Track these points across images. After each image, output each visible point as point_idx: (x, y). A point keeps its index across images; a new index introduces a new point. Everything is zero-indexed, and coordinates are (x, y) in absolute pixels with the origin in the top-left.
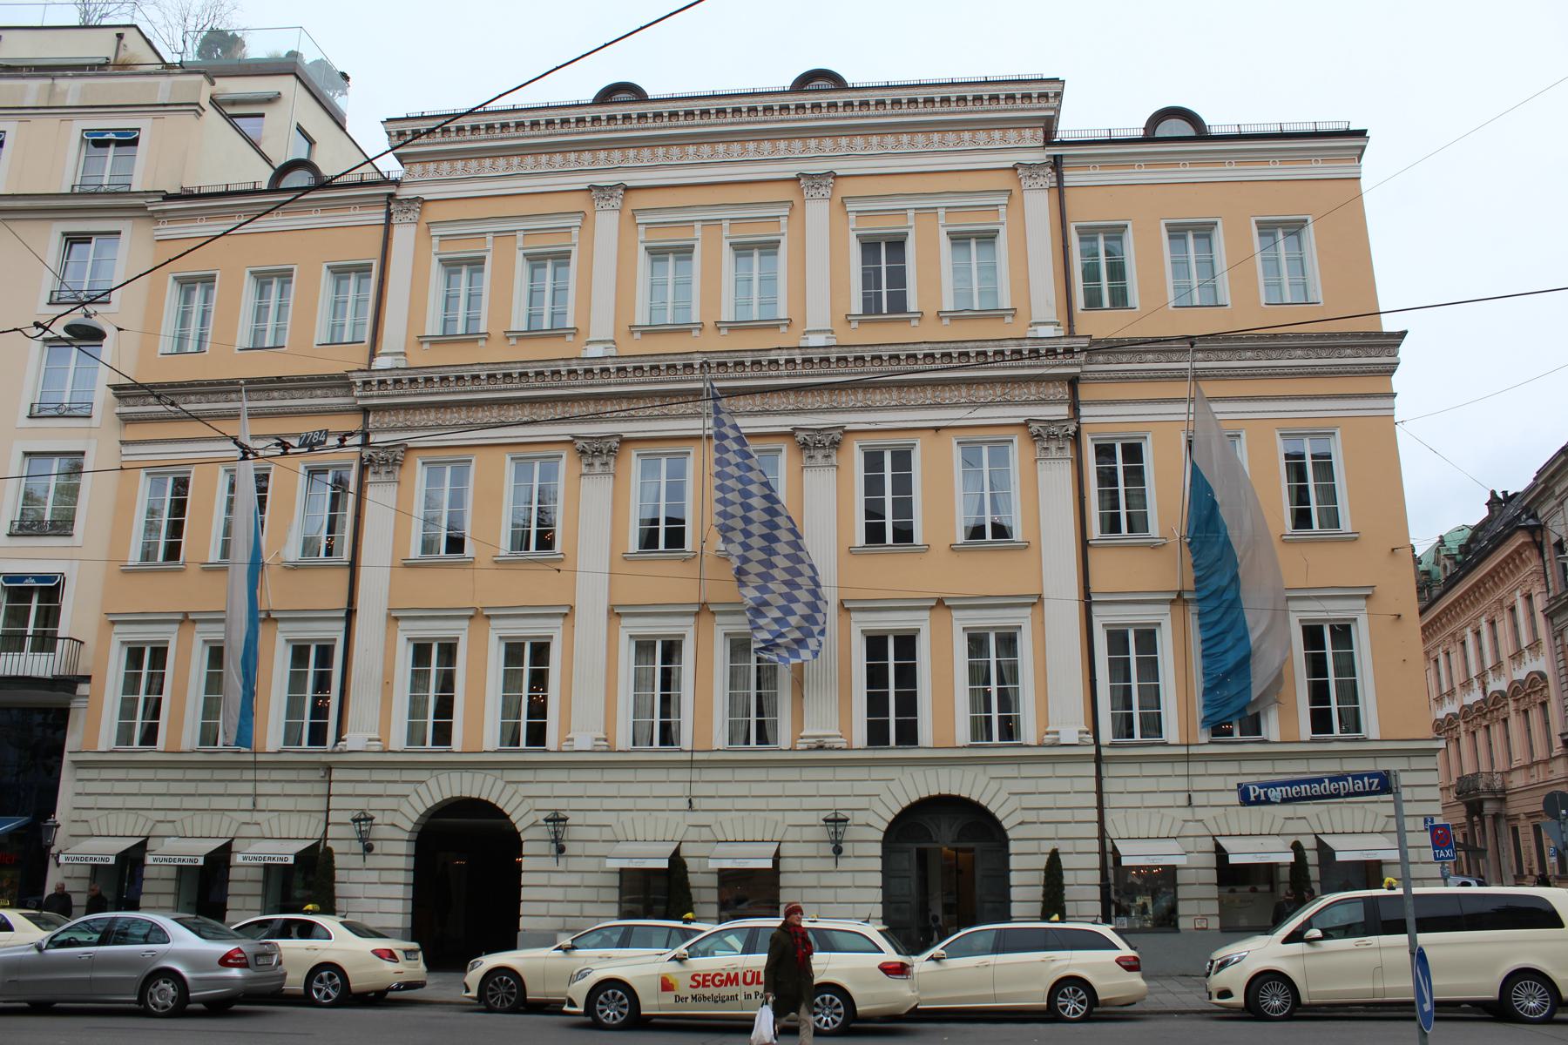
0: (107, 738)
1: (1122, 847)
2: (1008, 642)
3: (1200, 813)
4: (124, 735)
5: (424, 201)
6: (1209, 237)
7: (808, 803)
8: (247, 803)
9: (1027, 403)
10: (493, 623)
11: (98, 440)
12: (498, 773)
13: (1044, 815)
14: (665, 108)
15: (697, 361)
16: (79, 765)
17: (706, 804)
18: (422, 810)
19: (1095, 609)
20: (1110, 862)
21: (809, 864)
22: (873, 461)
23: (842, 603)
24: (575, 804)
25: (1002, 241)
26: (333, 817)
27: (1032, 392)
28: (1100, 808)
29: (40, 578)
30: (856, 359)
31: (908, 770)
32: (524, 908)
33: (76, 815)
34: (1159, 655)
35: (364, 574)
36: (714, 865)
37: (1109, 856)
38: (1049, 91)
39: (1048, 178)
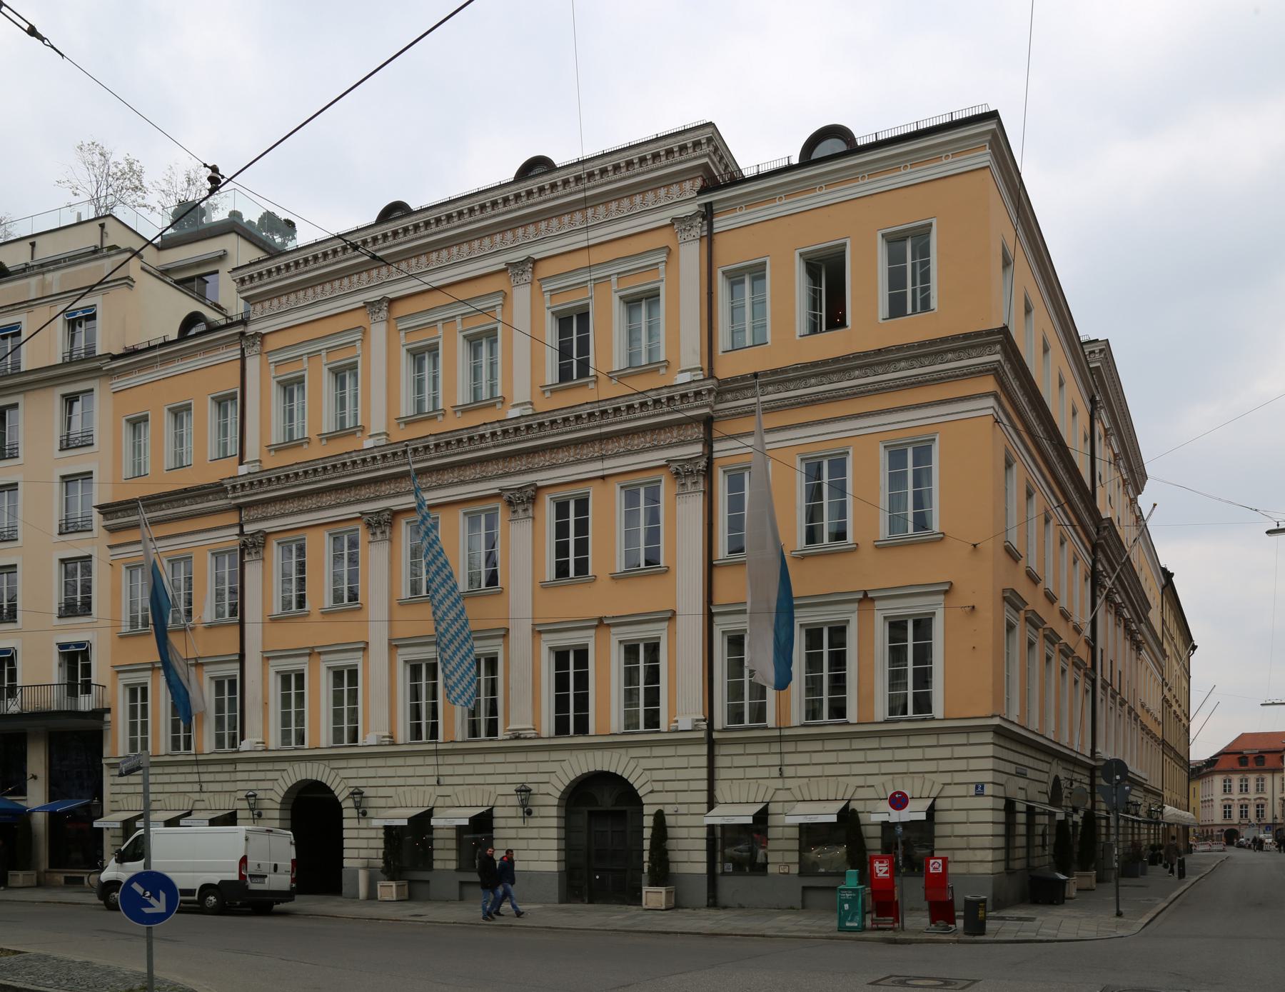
3: (789, 783)
8: (197, 788)
11: (94, 543)
13: (669, 786)
19: (717, 619)
21: (512, 823)
22: (562, 509)
23: (390, 640)
24: (372, 782)
31: (575, 753)
32: (346, 853)
35: (247, 627)
39: (698, 230)
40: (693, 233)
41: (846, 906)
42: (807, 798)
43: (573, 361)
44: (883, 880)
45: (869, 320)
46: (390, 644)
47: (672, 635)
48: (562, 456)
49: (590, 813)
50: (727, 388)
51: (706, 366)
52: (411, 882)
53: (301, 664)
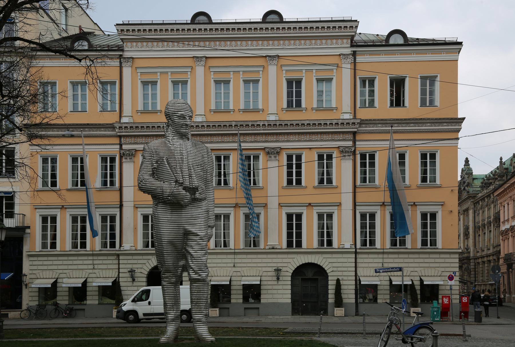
0: (38, 246)
1: (361, 279)
2: (330, 216)
4: (44, 246)
5: (133, 58)
7: (269, 265)
8: (91, 267)
9: (340, 140)
13: (339, 269)
15: (233, 124)
16: (30, 256)
17: (238, 265)
18: (150, 268)
19: (357, 207)
20: (358, 282)
21: (270, 283)
22: (290, 158)
23: (279, 204)
25: (334, 81)
26: (121, 270)
27: (341, 137)
28: (356, 267)
30: (285, 124)
33: (31, 272)
34: (437, 238)
36: (243, 283)
37: (357, 280)
38: (353, 24)
39: (351, 59)
41: (435, 313)
42: (42, 277)
43: (294, 100)
44: (446, 304)
45: (412, 105)
46: (134, 207)
47: (340, 211)
48: (292, 138)
49: (302, 279)
50: (363, 122)
51: (353, 112)
52: (220, 309)
53: (58, 213)
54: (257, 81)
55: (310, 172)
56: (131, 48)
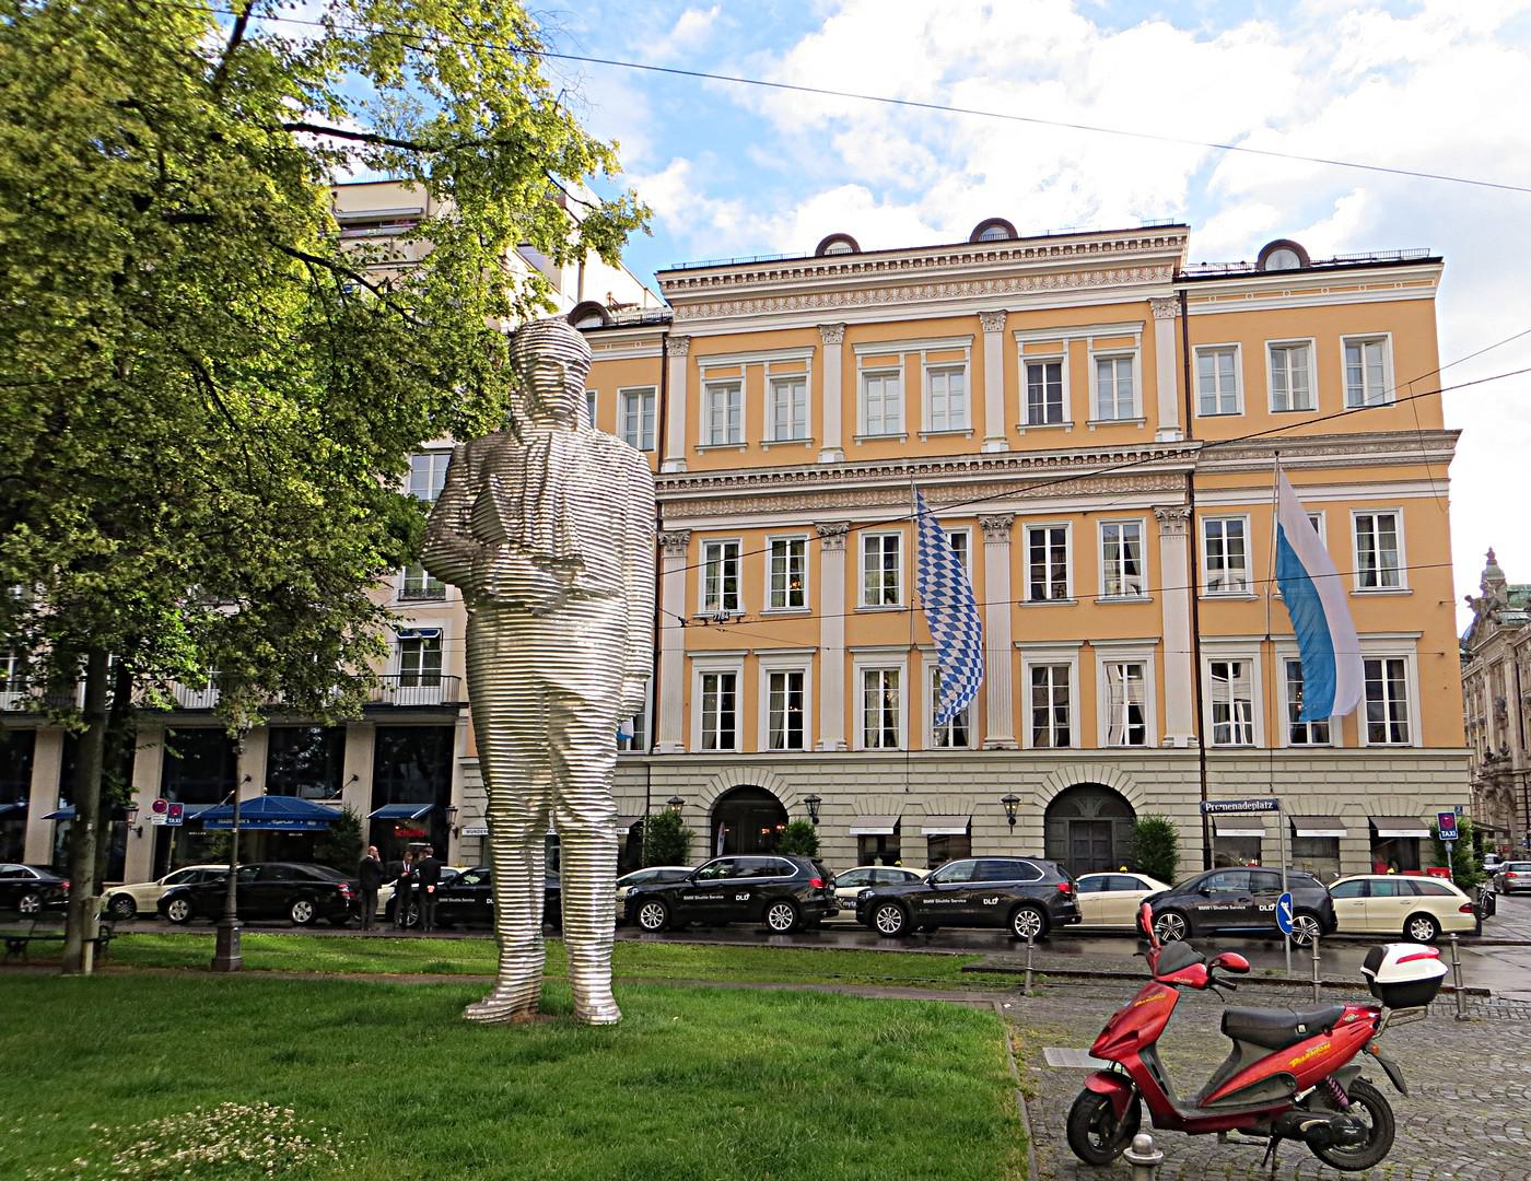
6: (1233, 356)
9: (1153, 492)
10: (761, 660)
12: (769, 768)
13: (1162, 799)
14: (874, 260)
19: (1202, 648)
22: (1037, 536)
23: (847, 649)
24: (826, 789)
25: (1137, 360)
29: (425, 632)
31: (1062, 765)
40: (1169, 312)
46: (685, 657)
49: (1072, 823)
54: (1129, 358)
55: (758, 578)
56: (688, 317)
